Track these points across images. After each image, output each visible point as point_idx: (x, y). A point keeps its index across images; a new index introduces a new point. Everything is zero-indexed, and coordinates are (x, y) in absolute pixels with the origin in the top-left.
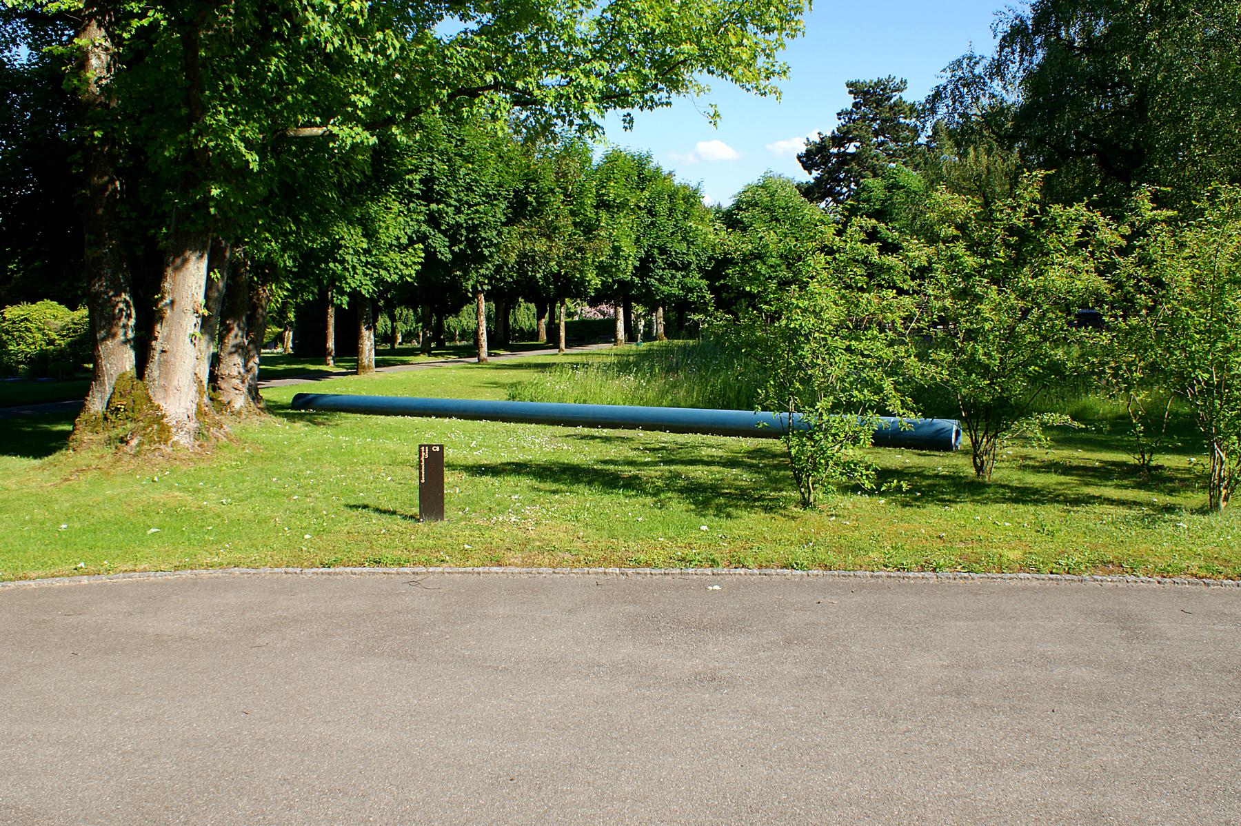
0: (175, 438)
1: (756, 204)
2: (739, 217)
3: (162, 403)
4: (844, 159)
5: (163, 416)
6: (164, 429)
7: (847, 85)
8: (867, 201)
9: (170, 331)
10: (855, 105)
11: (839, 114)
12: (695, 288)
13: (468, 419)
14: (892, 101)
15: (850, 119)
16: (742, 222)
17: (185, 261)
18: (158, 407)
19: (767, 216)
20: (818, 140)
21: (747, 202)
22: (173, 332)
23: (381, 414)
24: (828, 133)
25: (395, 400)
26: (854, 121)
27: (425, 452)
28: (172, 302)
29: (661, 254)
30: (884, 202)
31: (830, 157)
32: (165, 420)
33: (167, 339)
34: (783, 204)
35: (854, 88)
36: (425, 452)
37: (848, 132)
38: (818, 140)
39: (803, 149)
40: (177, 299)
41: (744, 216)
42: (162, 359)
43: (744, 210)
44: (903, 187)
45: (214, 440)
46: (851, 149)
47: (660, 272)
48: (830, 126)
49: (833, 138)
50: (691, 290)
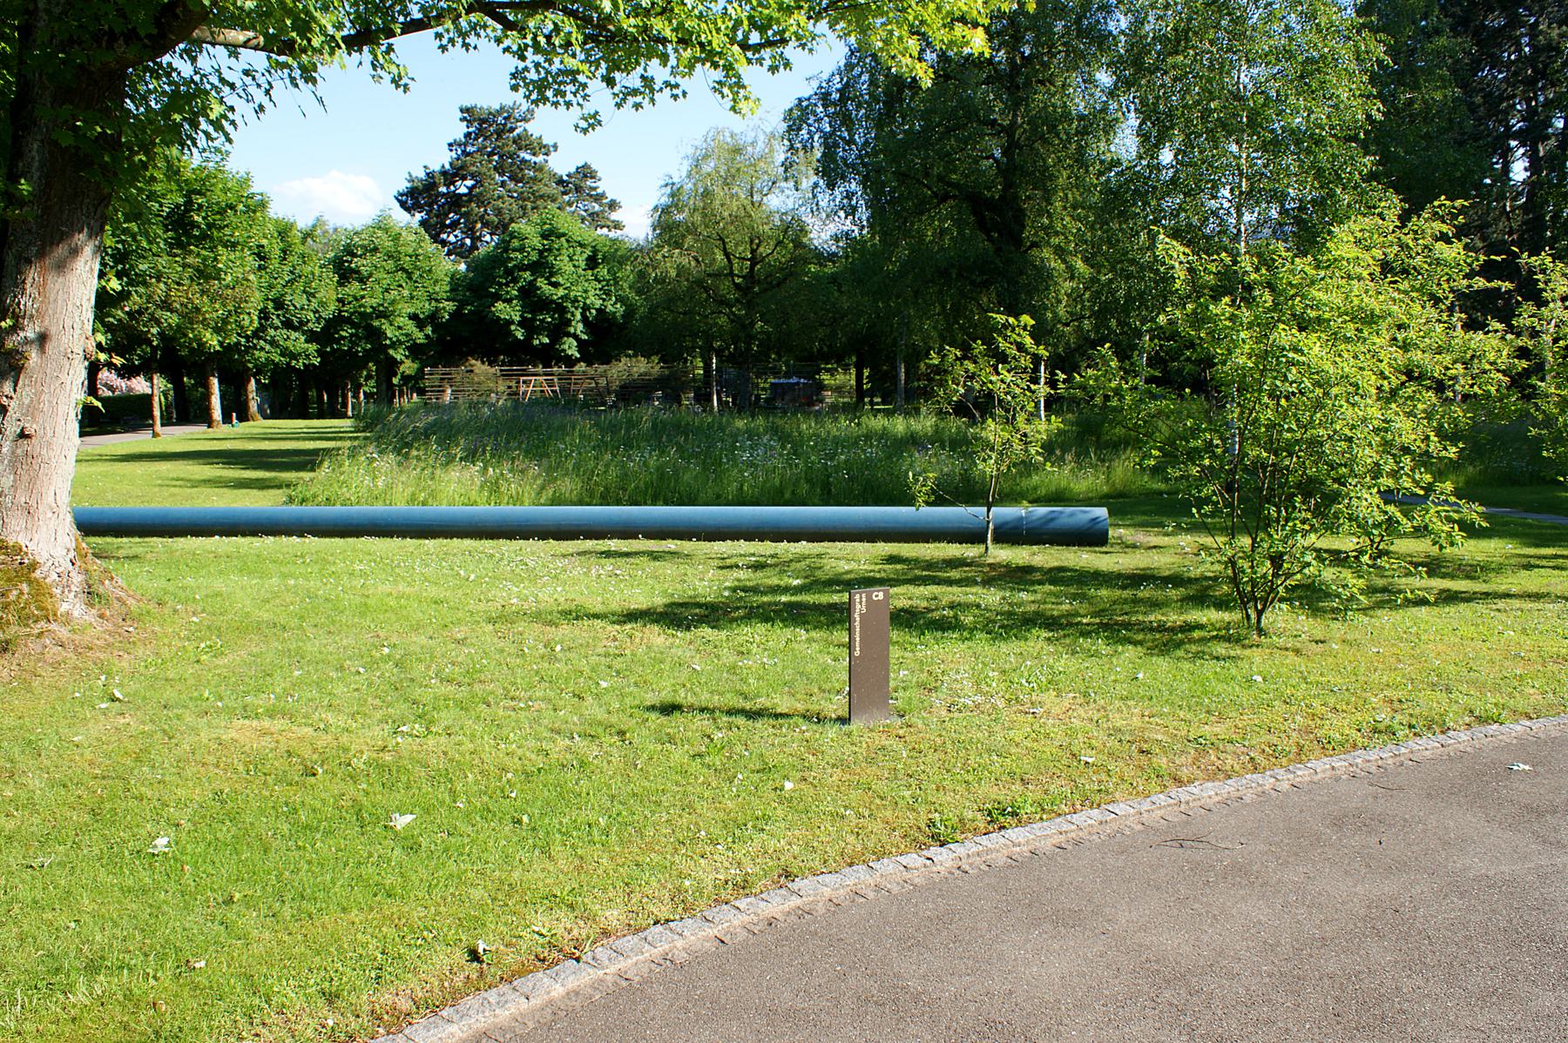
0: (64, 608)
1: (376, 250)
2: (353, 265)
3: (22, 541)
4: (455, 201)
5: (33, 566)
6: (39, 590)
7: (462, 111)
8: (521, 249)
9: (39, 394)
10: (468, 135)
11: (450, 145)
12: (300, 354)
13: (498, 538)
14: (515, 133)
15: (463, 152)
16: (358, 272)
17: (75, 252)
18: (18, 550)
19: (390, 265)
20: (422, 175)
21: (363, 247)
22: (45, 397)
23: (351, 536)
24: (437, 168)
25: (102, 512)
26: (468, 154)
27: (861, 603)
28: (43, 339)
29: (276, 309)
30: (541, 252)
31: (437, 197)
32: (37, 574)
33: (31, 410)
34: (410, 251)
35: (469, 114)
36: (861, 603)
37: (462, 168)
38: (422, 175)
39: (404, 185)
40: (53, 331)
41: (362, 264)
42: (19, 451)
43: (360, 256)
44: (564, 235)
45: (116, 605)
46: (462, 188)
47: (272, 332)
48: (442, 159)
49: (444, 173)
50: (294, 356)
